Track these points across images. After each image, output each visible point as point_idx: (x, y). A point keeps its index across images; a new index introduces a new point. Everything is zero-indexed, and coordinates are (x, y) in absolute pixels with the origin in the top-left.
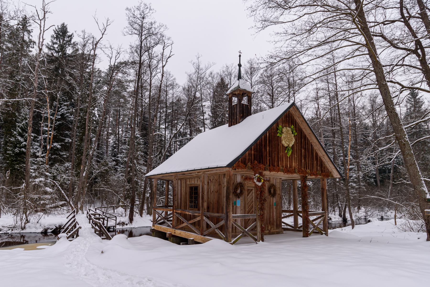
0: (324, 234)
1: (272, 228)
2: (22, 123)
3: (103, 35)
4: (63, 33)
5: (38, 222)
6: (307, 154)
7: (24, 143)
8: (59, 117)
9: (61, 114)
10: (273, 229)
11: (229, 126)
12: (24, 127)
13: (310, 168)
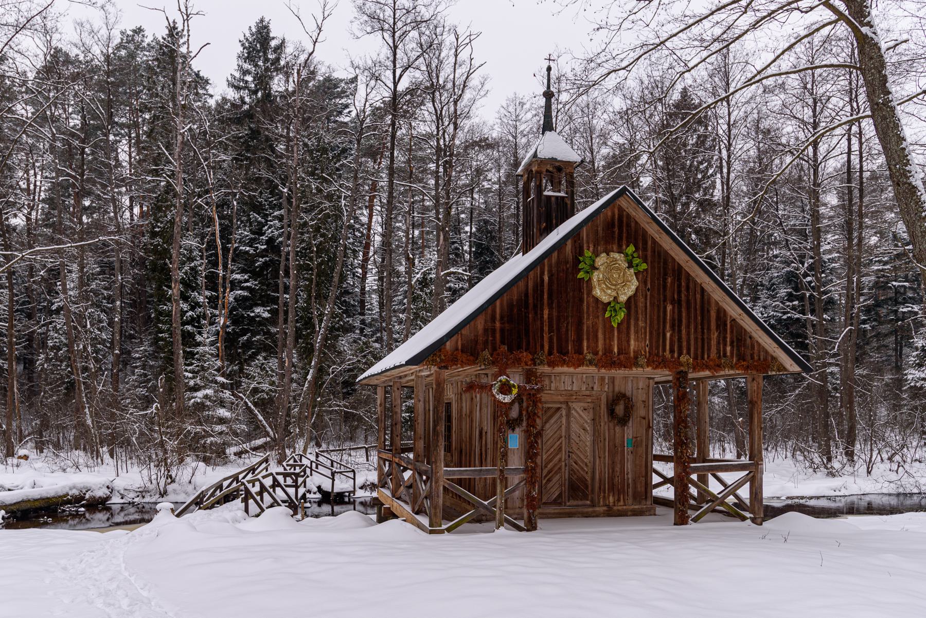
0: (749, 521)
1: (619, 500)
2: (183, 271)
3: (314, 45)
4: (262, 45)
5: (190, 482)
6: (684, 315)
7: (190, 313)
8: (263, 247)
9: (266, 240)
10: (622, 503)
11: (523, 255)
12: (189, 279)
13: (696, 349)
